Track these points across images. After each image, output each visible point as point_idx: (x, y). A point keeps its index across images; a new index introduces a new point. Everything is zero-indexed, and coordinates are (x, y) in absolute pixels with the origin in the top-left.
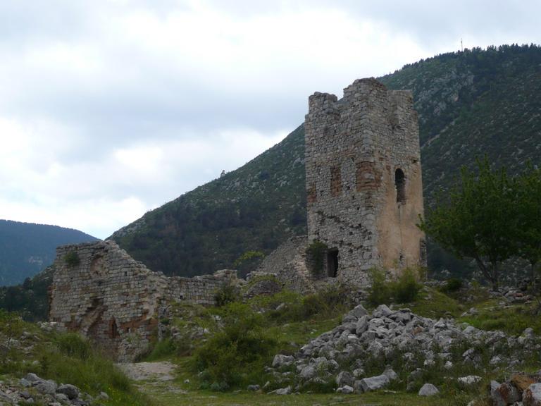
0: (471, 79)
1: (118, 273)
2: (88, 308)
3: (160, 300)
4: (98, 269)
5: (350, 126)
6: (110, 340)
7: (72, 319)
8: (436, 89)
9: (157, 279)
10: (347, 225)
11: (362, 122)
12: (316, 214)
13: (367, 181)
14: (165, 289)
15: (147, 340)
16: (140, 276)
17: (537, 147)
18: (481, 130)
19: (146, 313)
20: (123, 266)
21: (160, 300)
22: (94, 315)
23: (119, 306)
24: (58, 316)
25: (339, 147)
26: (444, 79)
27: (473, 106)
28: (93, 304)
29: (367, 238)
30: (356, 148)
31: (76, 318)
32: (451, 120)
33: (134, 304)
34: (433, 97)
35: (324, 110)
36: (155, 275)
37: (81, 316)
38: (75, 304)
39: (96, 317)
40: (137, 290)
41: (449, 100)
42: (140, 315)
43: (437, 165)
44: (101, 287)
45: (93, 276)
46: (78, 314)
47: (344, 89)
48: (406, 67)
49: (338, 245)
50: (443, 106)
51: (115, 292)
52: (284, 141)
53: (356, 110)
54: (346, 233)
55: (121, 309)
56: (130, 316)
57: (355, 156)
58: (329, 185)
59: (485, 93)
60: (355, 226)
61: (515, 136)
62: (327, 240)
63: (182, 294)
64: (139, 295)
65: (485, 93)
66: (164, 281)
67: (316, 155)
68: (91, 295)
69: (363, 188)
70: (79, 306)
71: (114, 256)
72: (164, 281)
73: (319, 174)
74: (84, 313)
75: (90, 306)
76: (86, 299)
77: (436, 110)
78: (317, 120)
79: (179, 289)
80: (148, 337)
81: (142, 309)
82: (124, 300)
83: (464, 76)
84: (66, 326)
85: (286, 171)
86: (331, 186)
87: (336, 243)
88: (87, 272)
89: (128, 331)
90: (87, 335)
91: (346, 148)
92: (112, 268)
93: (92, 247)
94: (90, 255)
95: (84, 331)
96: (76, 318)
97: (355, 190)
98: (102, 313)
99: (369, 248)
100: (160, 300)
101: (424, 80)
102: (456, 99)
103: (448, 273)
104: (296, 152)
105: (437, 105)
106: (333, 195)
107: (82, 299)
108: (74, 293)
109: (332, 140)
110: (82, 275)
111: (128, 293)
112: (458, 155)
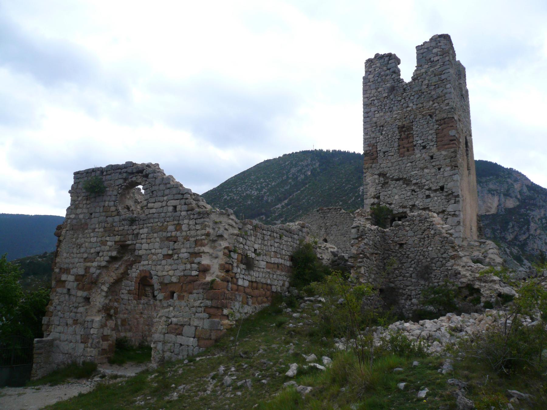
0: (317, 165)
1: (162, 207)
2: (111, 257)
3: (230, 251)
4: (130, 203)
5: (426, 82)
6: (135, 302)
7: (86, 272)
8: (300, 168)
9: (224, 219)
10: (421, 186)
11: (443, 77)
12: (377, 177)
13: (452, 138)
14: (237, 235)
15: (206, 315)
16: (199, 213)
17: (349, 202)
18: (321, 191)
19: (205, 270)
20: (171, 197)
21: (230, 251)
22: (120, 266)
23: (160, 256)
24: (65, 266)
25: (411, 105)
26: (305, 163)
27: (318, 178)
28: (118, 253)
29: (453, 201)
30: (436, 104)
32: (306, 184)
33: (186, 255)
34: (298, 171)
35: (389, 69)
36: (221, 214)
37: (99, 267)
38: (93, 251)
39: (121, 270)
40: (193, 233)
41: (306, 174)
42: (194, 273)
44: (134, 227)
45: (122, 211)
46: (95, 264)
47: (416, 47)
48: (285, 155)
49: (408, 210)
50: (302, 177)
51: (155, 235)
52: (218, 187)
53: (436, 65)
54: (420, 196)
55: (164, 262)
56: (179, 273)
57: (433, 113)
58: (396, 145)
59: (324, 172)
60: (434, 188)
61: (338, 195)
62: (390, 204)
63: (256, 246)
64: (196, 241)
65: (324, 172)
66: (234, 224)
67: (377, 115)
68: (117, 238)
69: (446, 147)
70: (98, 253)
71: (158, 182)
72: (234, 224)
73: (382, 134)
74: (104, 264)
75: (114, 254)
76: (109, 243)
77: (299, 178)
78: (379, 80)
79: (253, 238)
81: (199, 263)
82: (168, 248)
83: (314, 162)
84: (76, 280)
85: (219, 202)
86: (399, 146)
87: (405, 207)
88: (115, 206)
89: (172, 297)
90: (106, 297)
91: (421, 105)
92: (153, 200)
93: (123, 170)
94: (121, 181)
95: (102, 290)
96: (92, 270)
97: (434, 149)
98: (131, 265)
99: (457, 213)
100: (229, 251)
101: (294, 163)
102: (309, 174)
104: (225, 193)
106: (402, 155)
107: (104, 243)
108: (92, 234)
109: (399, 99)
110: (106, 210)
111: (176, 237)
112: (309, 202)
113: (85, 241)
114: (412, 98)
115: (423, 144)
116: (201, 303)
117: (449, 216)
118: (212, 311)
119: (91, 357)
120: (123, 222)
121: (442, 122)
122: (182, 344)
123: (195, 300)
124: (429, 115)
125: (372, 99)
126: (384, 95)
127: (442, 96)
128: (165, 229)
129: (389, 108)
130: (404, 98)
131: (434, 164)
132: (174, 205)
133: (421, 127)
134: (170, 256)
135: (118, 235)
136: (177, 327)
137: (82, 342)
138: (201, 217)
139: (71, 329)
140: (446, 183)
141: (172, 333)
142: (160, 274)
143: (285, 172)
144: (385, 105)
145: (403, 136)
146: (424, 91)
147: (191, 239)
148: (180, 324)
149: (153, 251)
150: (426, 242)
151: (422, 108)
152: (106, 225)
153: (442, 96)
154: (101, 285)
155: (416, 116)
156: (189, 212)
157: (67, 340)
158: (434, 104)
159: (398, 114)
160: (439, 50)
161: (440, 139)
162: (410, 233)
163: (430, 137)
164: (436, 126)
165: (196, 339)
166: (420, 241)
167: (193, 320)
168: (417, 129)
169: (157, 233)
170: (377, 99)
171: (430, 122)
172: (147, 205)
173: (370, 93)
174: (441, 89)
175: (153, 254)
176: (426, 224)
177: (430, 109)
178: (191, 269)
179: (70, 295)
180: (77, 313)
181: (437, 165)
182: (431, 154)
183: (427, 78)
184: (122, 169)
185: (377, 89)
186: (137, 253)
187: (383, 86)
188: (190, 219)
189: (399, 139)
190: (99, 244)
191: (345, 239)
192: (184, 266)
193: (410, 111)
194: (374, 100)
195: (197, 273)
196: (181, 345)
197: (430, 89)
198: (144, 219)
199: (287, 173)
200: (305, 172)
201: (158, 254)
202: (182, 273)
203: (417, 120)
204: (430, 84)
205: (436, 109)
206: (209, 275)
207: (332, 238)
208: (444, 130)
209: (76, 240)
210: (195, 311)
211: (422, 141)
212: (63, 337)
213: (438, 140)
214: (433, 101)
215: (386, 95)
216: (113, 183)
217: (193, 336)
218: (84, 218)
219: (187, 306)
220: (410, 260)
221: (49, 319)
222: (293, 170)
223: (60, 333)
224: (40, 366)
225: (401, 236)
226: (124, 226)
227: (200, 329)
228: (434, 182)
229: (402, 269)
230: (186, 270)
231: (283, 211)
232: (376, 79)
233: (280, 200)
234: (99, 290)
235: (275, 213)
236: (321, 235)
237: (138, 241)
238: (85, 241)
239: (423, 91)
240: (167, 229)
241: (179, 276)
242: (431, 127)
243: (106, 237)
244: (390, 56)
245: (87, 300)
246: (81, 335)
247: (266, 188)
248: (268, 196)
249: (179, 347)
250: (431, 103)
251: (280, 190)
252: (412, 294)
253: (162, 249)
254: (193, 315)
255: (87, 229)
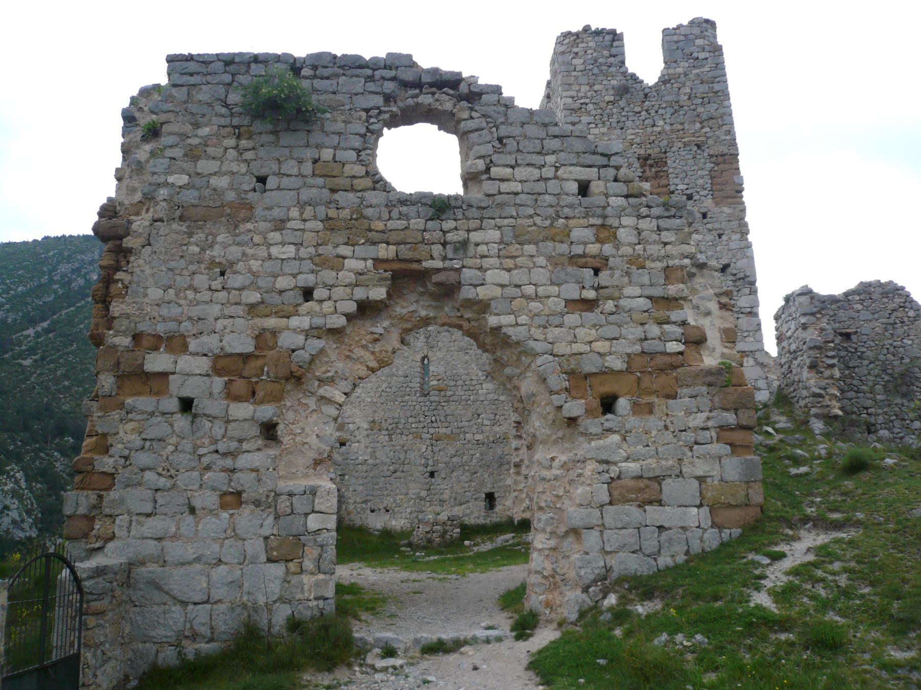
8: (77, 265)
31: (287, 340)
34: (73, 271)
40: (654, 249)
42: (674, 347)
43: (70, 335)
44: (449, 225)
46: (301, 322)
48: (46, 238)
50: (81, 281)
51: (530, 249)
53: (702, 66)
55: (572, 319)
69: (730, 200)
76: (350, 263)
77: (73, 285)
80: (727, 435)
91: (680, 127)
96: (287, 340)
97: (708, 203)
102: (95, 278)
103: (72, 440)
105: (75, 279)
109: (637, 109)
113: (244, 254)
114: (661, 112)
115: (688, 192)
116: (708, 418)
117: (741, 315)
118: (738, 436)
119: (321, 603)
120: (404, 209)
121: (720, 159)
122: (666, 525)
123: (688, 413)
124: (696, 145)
125: (582, 101)
126: (607, 98)
127: (717, 118)
128: (565, 235)
129: (618, 122)
130: (647, 111)
131: (709, 226)
132: (583, 178)
133: (682, 163)
134: (589, 305)
135: (388, 244)
136: (641, 484)
137: (270, 560)
138: (672, 213)
139: (211, 525)
140: (734, 260)
141: (626, 501)
142: (562, 348)
143: (45, 269)
144: (610, 116)
145: (648, 173)
146: (684, 104)
147: (648, 264)
148: (651, 475)
149: (530, 290)
150: (900, 331)
151: (681, 132)
152: (332, 213)
153: (717, 118)
154: (319, 386)
155: (670, 145)
156: (632, 200)
157: (198, 559)
158: (702, 128)
159: (636, 134)
160: (706, 42)
161: (718, 187)
162: (865, 315)
163: (700, 182)
164: (709, 166)
165: (705, 510)
166: (886, 330)
167: (692, 463)
168: (674, 165)
169: (536, 244)
170: (594, 103)
171: (698, 157)
172: (488, 170)
173: (578, 91)
174: (715, 106)
175: (528, 298)
176: (897, 300)
177: (696, 135)
178: (664, 338)
179: (195, 416)
180: (233, 471)
181: (716, 230)
182: (703, 210)
183: (688, 83)
184: (374, 70)
185: (592, 86)
186: (467, 293)
187: (604, 82)
188: (640, 217)
189: (640, 177)
190: (308, 265)
191: (467, 357)
192: (640, 328)
193: (659, 133)
194: (586, 104)
195: (681, 348)
196: (661, 528)
197: (695, 102)
198: (483, 205)
199: (50, 272)
200: (87, 274)
201: (548, 297)
202: (637, 348)
203: (673, 149)
204: (693, 95)
205: (708, 138)
206: (707, 353)
207: (440, 355)
208: (724, 174)
209: (203, 250)
210: (693, 439)
211: (686, 187)
212: (175, 551)
213: (714, 188)
214: (701, 123)
215: (612, 98)
216: (347, 101)
217: (698, 503)
218: (231, 187)
219: (666, 428)
220: (865, 362)
221: (100, 497)
222: (64, 268)
223: (159, 539)
224: (104, 653)
225: (845, 319)
226: (408, 219)
227: (716, 482)
228: (712, 256)
229: (853, 378)
230: (646, 339)
231: (37, 343)
232: (588, 68)
233: (33, 322)
234: (312, 402)
235: (20, 344)
236: (417, 349)
237: (468, 262)
238: (244, 254)
239: (681, 103)
240: (568, 235)
241: (629, 355)
242: (701, 165)
243: (337, 246)
244: (613, 32)
245: (269, 431)
246: (266, 538)
247: (4, 296)
248: (8, 311)
249: (656, 535)
250: (698, 125)
251: (33, 302)
252: (879, 422)
253: (559, 285)
254: (686, 449)
255: (247, 220)
